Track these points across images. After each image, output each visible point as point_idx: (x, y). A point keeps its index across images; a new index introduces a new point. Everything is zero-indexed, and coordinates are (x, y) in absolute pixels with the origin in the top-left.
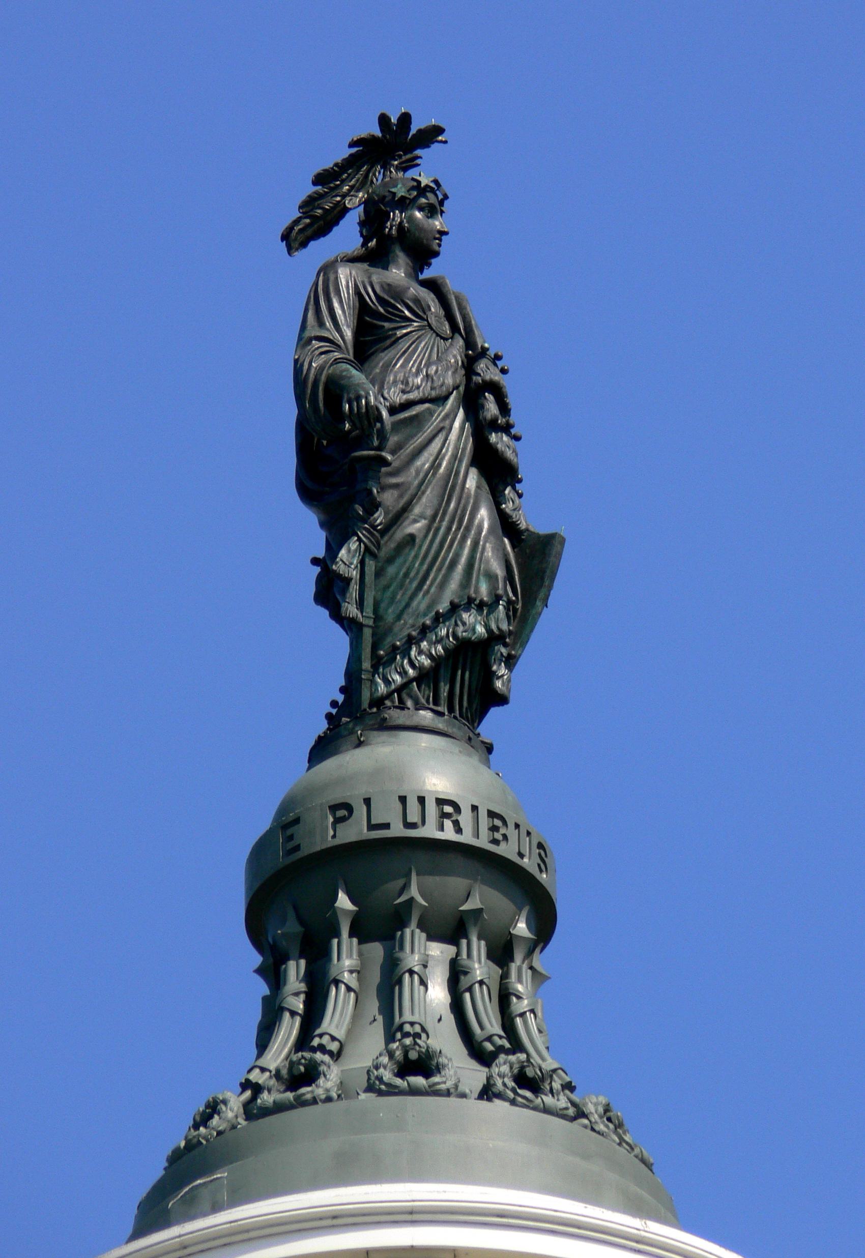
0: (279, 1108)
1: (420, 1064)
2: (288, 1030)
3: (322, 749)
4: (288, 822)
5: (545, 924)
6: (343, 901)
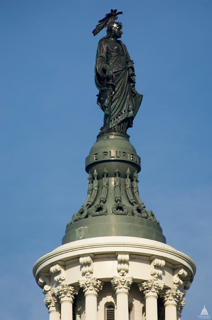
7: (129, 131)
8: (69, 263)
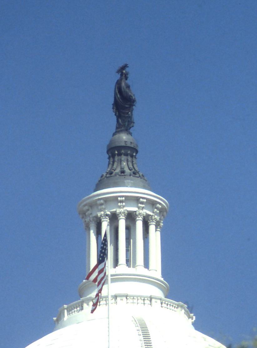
0: (109, 177)
1: (123, 172)
2: (110, 166)
3: (114, 134)
4: (111, 142)
5: (137, 152)
6: (116, 152)
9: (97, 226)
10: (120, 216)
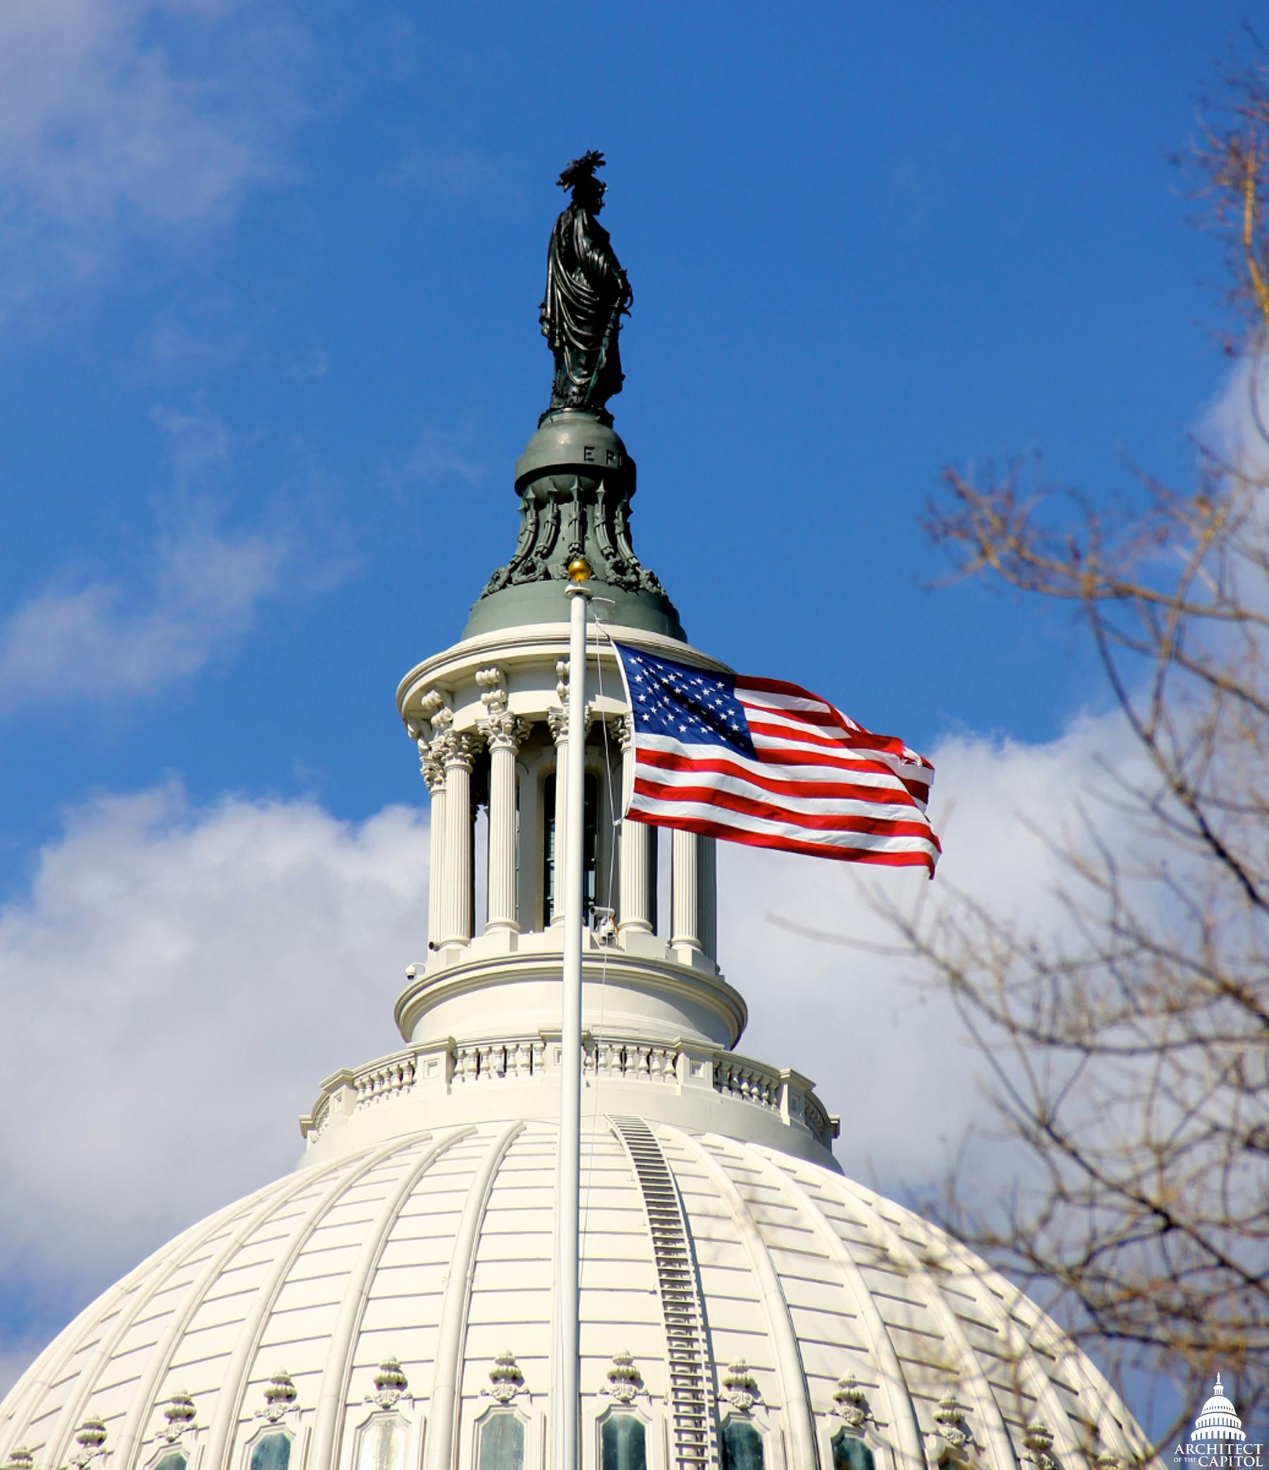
7: (612, 405)
8: (456, 691)
9: (146, 806)
10: (494, 740)
